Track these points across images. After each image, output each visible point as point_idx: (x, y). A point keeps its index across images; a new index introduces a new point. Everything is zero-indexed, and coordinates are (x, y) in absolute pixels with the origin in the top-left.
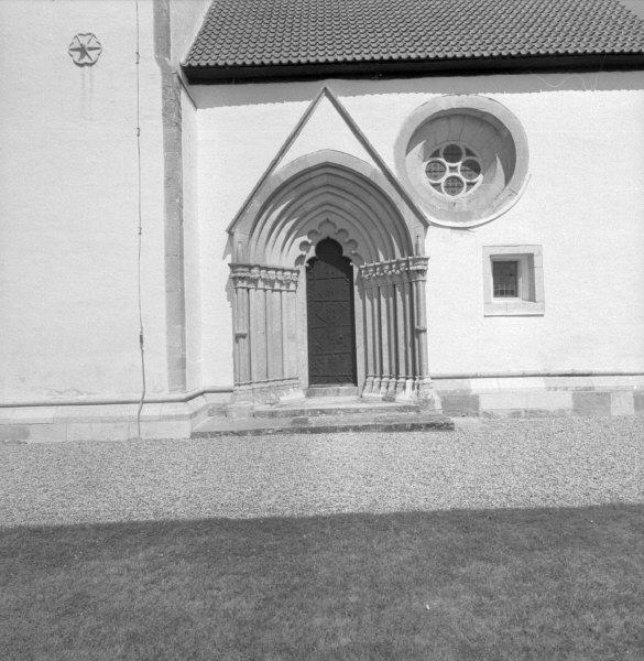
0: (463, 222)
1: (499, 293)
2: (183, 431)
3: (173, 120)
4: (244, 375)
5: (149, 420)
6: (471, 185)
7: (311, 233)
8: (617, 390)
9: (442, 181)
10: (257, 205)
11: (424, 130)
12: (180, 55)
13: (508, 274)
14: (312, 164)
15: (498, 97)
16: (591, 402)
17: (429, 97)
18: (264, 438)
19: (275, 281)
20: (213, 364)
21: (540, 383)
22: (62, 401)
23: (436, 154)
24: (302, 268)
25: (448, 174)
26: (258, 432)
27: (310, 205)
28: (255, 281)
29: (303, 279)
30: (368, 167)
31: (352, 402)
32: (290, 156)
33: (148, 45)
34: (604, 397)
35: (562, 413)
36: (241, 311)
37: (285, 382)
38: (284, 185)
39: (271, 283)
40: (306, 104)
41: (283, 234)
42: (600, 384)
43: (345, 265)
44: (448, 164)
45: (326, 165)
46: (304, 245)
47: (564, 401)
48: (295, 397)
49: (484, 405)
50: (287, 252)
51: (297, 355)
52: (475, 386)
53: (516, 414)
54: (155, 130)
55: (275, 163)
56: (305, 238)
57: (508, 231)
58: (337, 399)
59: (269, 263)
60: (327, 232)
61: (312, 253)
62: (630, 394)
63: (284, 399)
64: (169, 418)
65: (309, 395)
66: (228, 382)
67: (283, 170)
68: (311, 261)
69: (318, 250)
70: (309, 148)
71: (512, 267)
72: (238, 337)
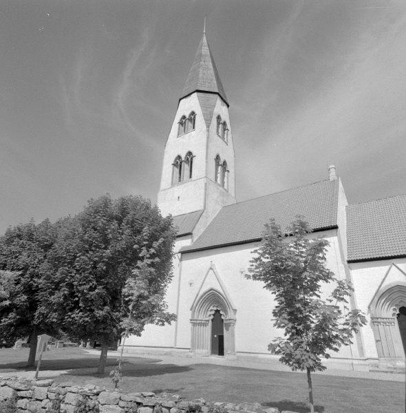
2: (367, 369)
3: (177, 312)
4: (381, 354)
5: (355, 365)
7: (396, 305)
10: (376, 299)
14: (393, 286)
16: (228, 326)
18: (393, 374)
19: (386, 322)
22: (336, 357)
24: (395, 317)
26: (392, 372)
27: (395, 297)
28: (379, 323)
29: (396, 321)
32: (386, 283)
36: (377, 333)
37: (396, 358)
39: (385, 323)
41: (386, 306)
50: (207, 316)
54: (179, 312)
55: (380, 286)
59: (383, 317)
61: (398, 312)
63: (398, 364)
64: (361, 365)
66: (376, 356)
67: (383, 288)
68: (398, 315)
72: (377, 341)
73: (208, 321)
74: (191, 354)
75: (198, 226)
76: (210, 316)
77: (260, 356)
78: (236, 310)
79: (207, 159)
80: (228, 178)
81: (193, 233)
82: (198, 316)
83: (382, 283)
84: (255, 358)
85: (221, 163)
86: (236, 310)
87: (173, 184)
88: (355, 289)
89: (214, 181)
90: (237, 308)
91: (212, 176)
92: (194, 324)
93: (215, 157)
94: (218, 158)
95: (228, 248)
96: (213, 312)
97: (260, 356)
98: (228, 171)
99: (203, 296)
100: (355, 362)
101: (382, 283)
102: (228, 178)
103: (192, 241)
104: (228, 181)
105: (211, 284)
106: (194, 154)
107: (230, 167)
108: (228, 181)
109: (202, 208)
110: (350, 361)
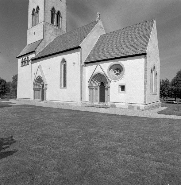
0: (115, 79)
1: (122, 90)
6: (120, 74)
8: (135, 106)
9: (116, 74)
10: (91, 79)
11: (111, 67)
12: (84, 61)
13: (123, 88)
15: (121, 62)
16: (107, 89)
17: (111, 63)
19: (95, 88)
20: (86, 98)
21: (124, 104)
23: (115, 70)
24: (99, 86)
25: (118, 72)
29: (99, 88)
30: (103, 73)
31: (160, 113)
33: (79, 62)
34: (133, 107)
35: (127, 109)
38: (94, 76)
40: (96, 65)
42: (132, 105)
43: (104, 85)
44: (117, 71)
45: (122, 67)
46: (99, 83)
47: (127, 107)
48: (97, 103)
49: (116, 106)
50: (97, 84)
51: (98, 98)
52: (116, 104)
53: (120, 108)
56: (99, 82)
57: (121, 82)
58: (102, 104)
60: (102, 81)
61: (100, 84)
62: (137, 107)
65: (99, 103)
67: (94, 75)
68: (100, 85)
69: (101, 84)
70: (96, 72)
71: (14, 97)
73: (40, 89)
74: (33, 101)
75: (38, 47)
76: (41, 86)
77: (53, 101)
78: (47, 84)
79: (44, 10)
80: (61, 21)
81: (36, 51)
82: (93, 85)
83: (94, 72)
84: (52, 102)
85: (56, 12)
86: (47, 84)
87: (32, 25)
88: (12, 78)
89: (50, 23)
90: (47, 83)
91: (49, 20)
92: (34, 90)
93: (51, 9)
94: (53, 10)
95: (137, 57)
96: (42, 85)
97: (53, 101)
98: (61, 17)
99: (37, 79)
100: (78, 103)
101: (94, 72)
102: (61, 21)
103: (35, 55)
104: (61, 23)
105: (39, 74)
106: (40, 8)
107: (64, 15)
108: (61, 23)
109: (42, 38)
110: (76, 103)
